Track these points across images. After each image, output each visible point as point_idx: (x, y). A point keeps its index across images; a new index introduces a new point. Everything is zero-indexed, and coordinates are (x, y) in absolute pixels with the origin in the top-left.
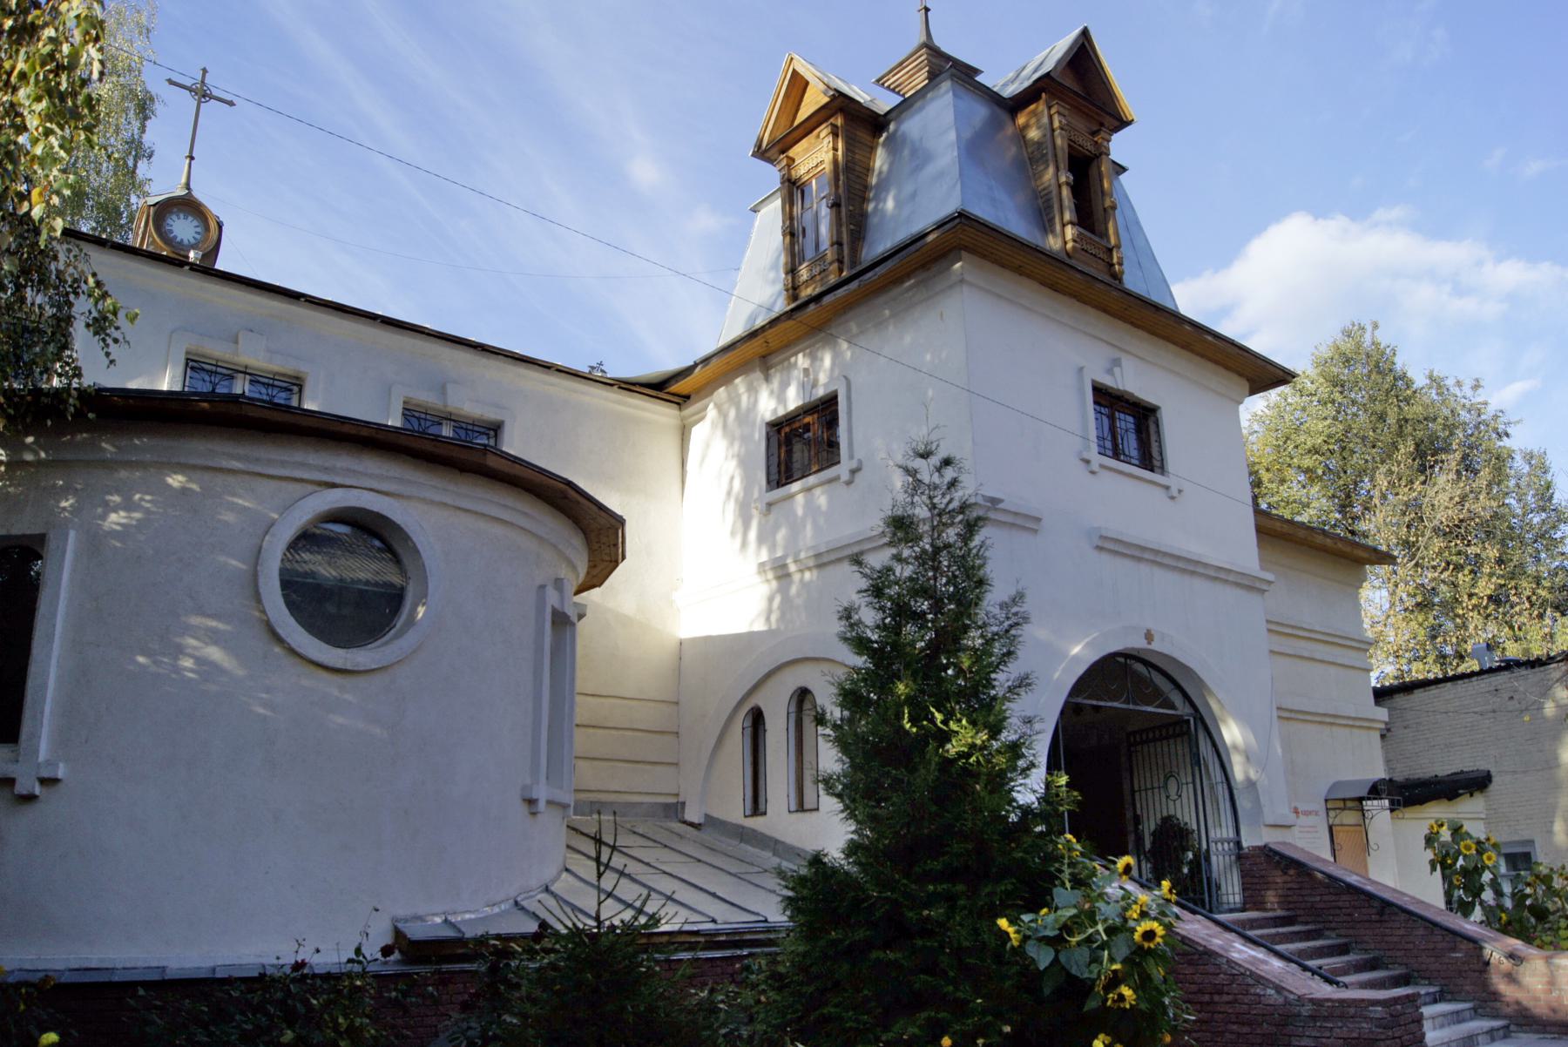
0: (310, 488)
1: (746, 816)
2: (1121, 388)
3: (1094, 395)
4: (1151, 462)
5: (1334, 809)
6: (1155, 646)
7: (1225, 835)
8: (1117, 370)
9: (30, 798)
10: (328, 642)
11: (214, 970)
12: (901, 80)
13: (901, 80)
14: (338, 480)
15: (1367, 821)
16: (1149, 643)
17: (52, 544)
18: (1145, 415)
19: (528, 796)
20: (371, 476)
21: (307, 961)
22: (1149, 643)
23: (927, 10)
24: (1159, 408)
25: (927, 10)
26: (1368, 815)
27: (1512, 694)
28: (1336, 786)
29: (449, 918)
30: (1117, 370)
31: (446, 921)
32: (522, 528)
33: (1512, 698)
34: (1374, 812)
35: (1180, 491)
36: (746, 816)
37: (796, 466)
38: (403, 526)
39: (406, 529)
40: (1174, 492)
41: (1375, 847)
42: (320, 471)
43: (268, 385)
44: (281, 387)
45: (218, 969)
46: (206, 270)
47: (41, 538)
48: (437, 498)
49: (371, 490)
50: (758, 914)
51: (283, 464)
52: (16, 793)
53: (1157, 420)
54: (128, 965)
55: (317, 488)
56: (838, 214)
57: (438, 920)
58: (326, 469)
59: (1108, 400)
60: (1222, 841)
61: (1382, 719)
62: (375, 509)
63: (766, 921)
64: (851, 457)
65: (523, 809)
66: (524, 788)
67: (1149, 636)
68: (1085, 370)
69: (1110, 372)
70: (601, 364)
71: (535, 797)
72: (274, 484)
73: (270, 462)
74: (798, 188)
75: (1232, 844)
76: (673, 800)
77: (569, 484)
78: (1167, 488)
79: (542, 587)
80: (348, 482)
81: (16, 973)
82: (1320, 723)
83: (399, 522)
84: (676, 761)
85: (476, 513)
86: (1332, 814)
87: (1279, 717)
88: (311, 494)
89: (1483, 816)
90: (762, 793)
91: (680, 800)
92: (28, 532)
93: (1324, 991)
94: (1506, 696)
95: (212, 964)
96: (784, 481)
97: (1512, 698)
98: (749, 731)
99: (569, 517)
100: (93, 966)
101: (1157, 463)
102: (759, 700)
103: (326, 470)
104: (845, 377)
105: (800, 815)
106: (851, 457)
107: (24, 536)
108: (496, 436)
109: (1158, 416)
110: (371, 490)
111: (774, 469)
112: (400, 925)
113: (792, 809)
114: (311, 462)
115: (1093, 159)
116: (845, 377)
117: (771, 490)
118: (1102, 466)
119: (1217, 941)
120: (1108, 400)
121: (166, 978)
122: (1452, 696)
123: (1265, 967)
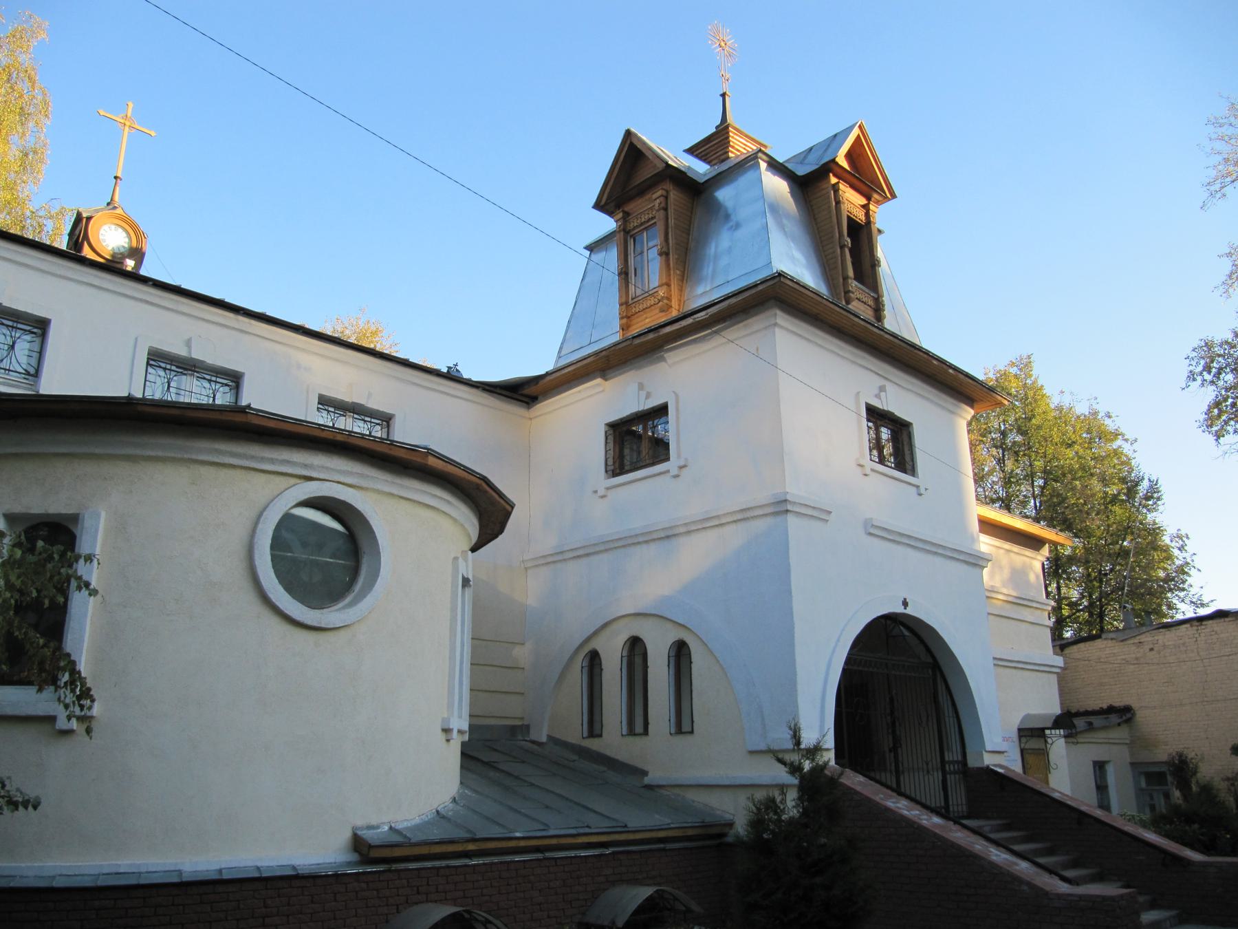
0: (293, 481)
1: (583, 738)
2: (886, 409)
3: (867, 414)
4: (905, 465)
5: (1025, 736)
6: (909, 611)
7: (955, 759)
8: (883, 394)
9: (68, 733)
10: (302, 602)
11: (220, 871)
12: (708, 151)
13: (708, 151)
14: (314, 475)
15: (1048, 746)
16: (905, 609)
17: (87, 522)
18: (900, 430)
19: (446, 727)
20: (340, 472)
21: (16, 812)
22: (905, 609)
23: (723, 95)
24: (912, 424)
25: (723, 95)
26: (1049, 741)
27: (1152, 646)
28: (1027, 717)
29: (393, 825)
30: (883, 394)
31: (391, 828)
32: (443, 512)
33: (1152, 649)
34: (1054, 739)
35: (926, 489)
36: (583, 738)
37: (627, 462)
38: (363, 512)
39: (365, 514)
40: (922, 491)
41: (1054, 767)
42: (301, 467)
43: (13, 327)
44: (25, 330)
45: (223, 871)
46: (135, 277)
47: (75, 518)
48: (387, 489)
49: (338, 482)
50: (614, 820)
51: (272, 461)
52: (57, 728)
53: (910, 433)
54: (150, 870)
55: (298, 481)
56: (667, 261)
57: (386, 828)
58: (306, 465)
59: (876, 416)
60: (953, 762)
61: (1060, 665)
62: (342, 498)
63: (626, 826)
64: (679, 456)
65: (442, 737)
66: (443, 720)
67: (905, 604)
68: (860, 394)
69: (878, 396)
70: (456, 365)
71: (451, 727)
72: (263, 477)
73: (262, 459)
74: (631, 236)
75: (960, 766)
76: (518, 723)
77: (485, 479)
78: (918, 487)
79: (456, 559)
80: (322, 476)
81: (58, 878)
82: (1015, 668)
83: (360, 509)
84: (522, 692)
85: (414, 501)
86: (1024, 740)
87: (995, 665)
88: (294, 485)
89: (1128, 742)
90: (596, 718)
91: (526, 723)
92: (64, 511)
93: (1064, 888)
94: (1147, 647)
95: (218, 867)
96: (618, 471)
97: (1152, 649)
98: (586, 670)
99: (473, 502)
100: (122, 871)
101: (909, 467)
102: (597, 644)
103: (306, 466)
104: (674, 392)
105: (631, 739)
106: (679, 456)
107: (60, 515)
108: (388, 426)
109: (911, 430)
110: (338, 482)
111: (610, 462)
112: (359, 833)
113: (624, 733)
114: (295, 460)
115: (632, 144)
116: (674, 392)
117: (608, 478)
118: (873, 470)
119: (978, 847)
120: (876, 416)
121: (184, 880)
122: (1104, 646)
123: (1017, 868)
